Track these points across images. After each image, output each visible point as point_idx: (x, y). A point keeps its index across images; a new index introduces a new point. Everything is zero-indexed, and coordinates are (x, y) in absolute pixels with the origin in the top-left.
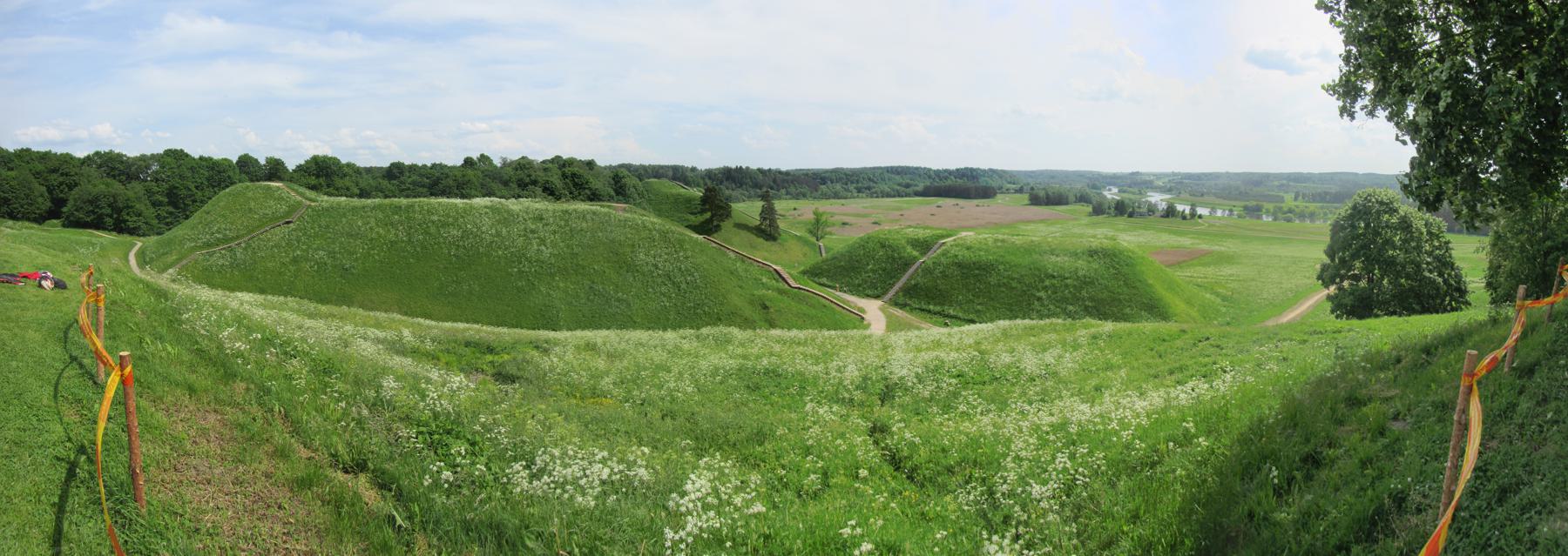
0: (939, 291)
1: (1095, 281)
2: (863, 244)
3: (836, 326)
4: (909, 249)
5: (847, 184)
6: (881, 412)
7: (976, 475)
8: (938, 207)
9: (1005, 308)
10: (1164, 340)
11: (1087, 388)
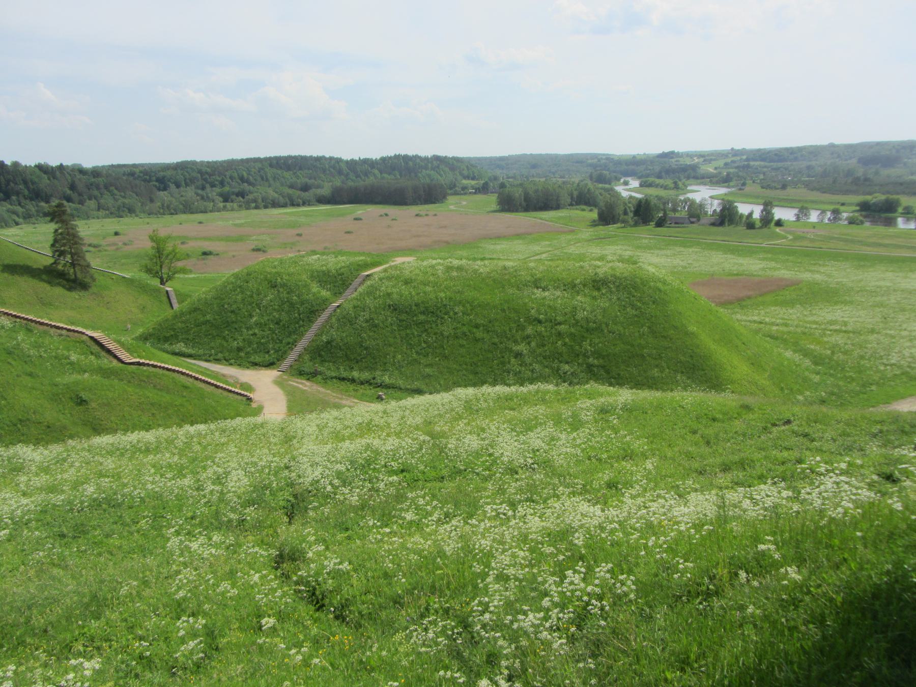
0: (366, 349)
1: (604, 326)
2: (241, 283)
3: (207, 416)
4: (315, 288)
5: (203, 188)
6: (288, 533)
7: (436, 606)
8: (356, 219)
9: (466, 370)
10: (714, 420)
11: (596, 485)
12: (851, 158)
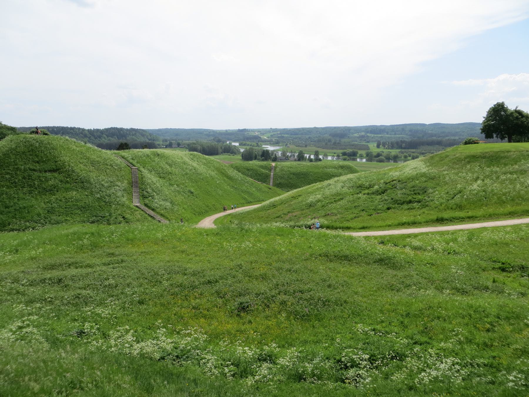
12: (325, 134)
